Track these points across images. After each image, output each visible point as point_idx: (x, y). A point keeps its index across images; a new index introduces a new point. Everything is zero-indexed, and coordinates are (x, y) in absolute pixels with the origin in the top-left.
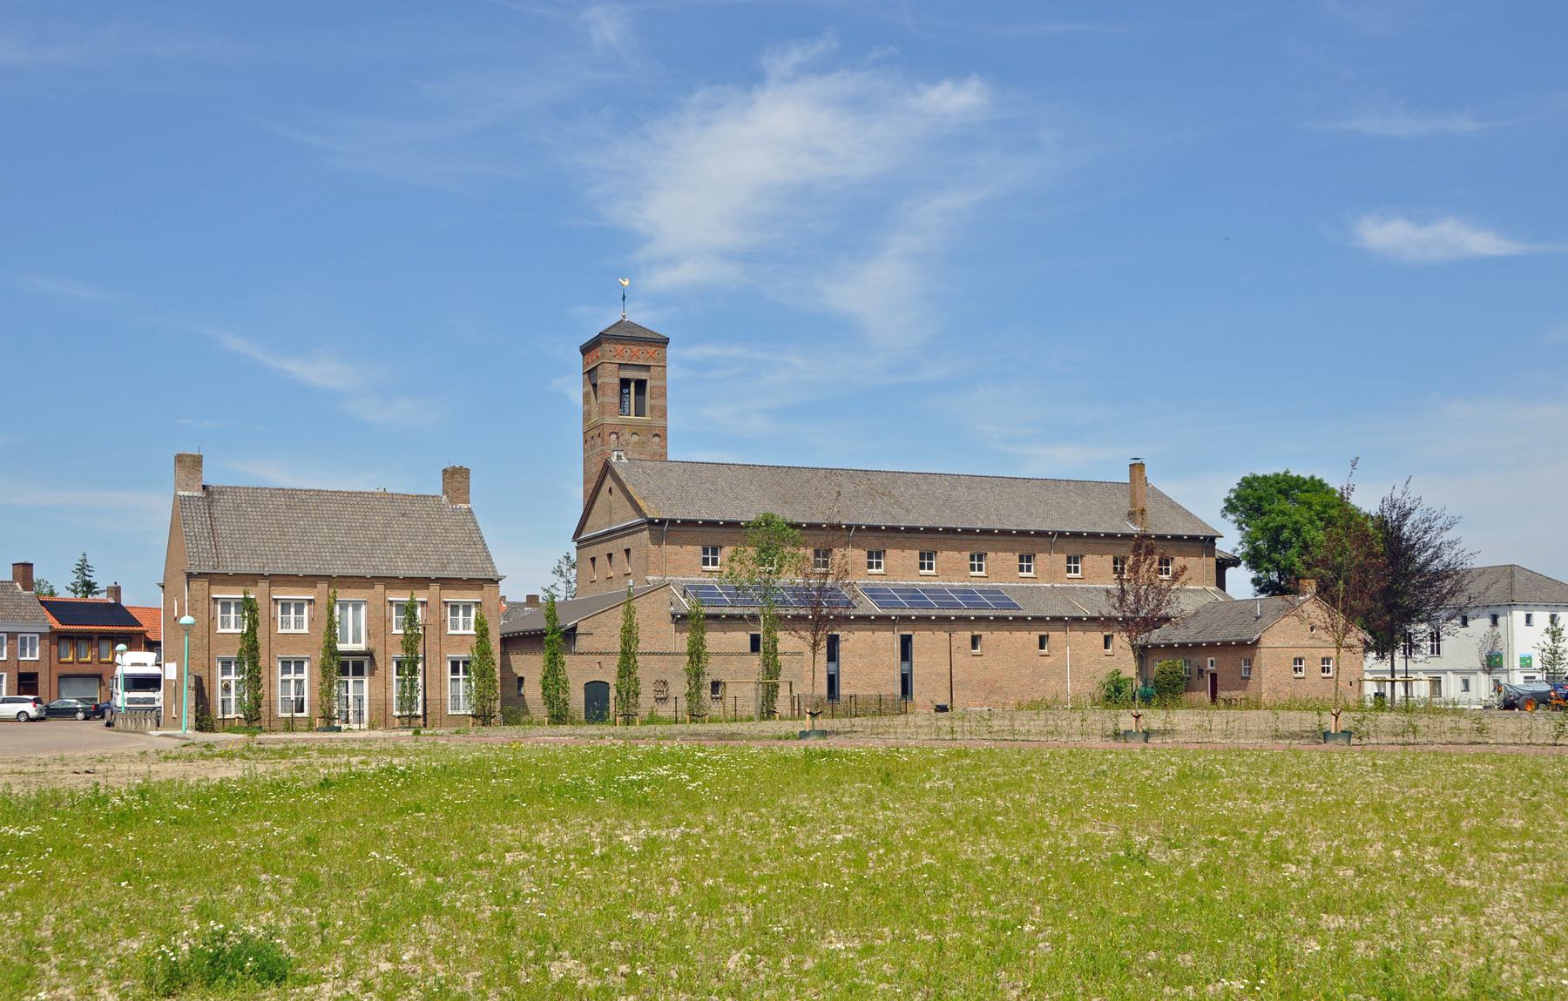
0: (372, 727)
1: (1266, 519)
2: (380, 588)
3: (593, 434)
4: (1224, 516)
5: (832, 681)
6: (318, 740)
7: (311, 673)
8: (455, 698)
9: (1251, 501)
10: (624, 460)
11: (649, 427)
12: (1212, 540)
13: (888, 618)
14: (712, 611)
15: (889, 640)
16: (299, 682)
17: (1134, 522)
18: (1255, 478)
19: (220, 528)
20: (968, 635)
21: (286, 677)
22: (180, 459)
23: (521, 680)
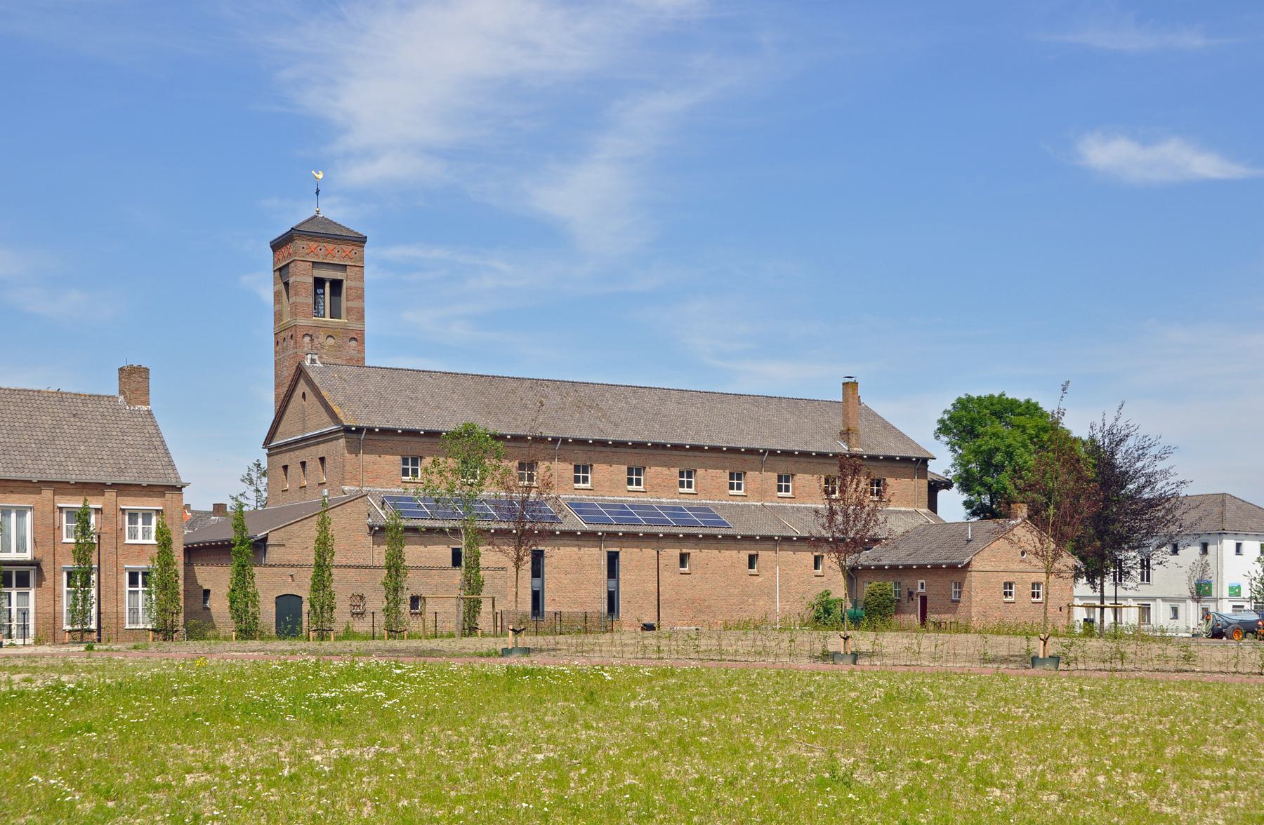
2: (47, 493)
4: (937, 438)
5: (537, 597)
8: (134, 611)
9: (965, 423)
10: (319, 364)
11: (345, 330)
12: (924, 461)
14: (411, 523)
15: (596, 556)
20: (744, 556)
23: (207, 592)
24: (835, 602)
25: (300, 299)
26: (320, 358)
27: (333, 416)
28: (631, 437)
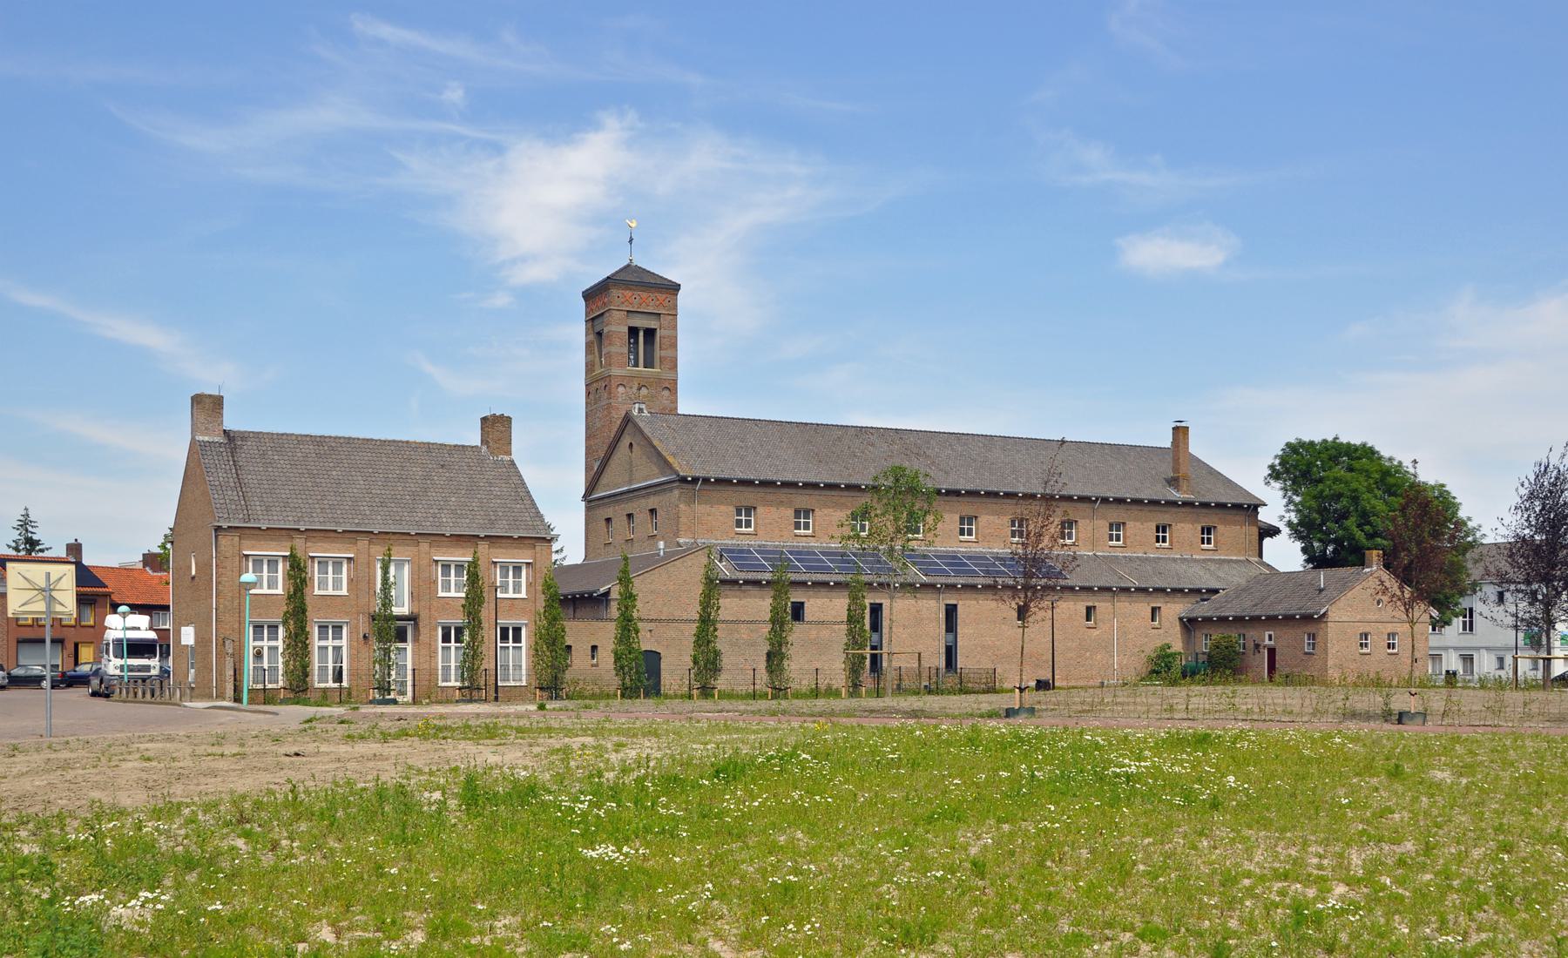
0: (415, 701)
1: (1320, 486)
2: (424, 546)
3: (597, 387)
4: (1267, 483)
5: (950, 653)
6: (461, 715)
7: (350, 640)
8: (446, 669)
9: (1301, 466)
10: (646, 413)
12: (1256, 507)
13: (933, 586)
14: (751, 576)
15: (933, 608)
16: (337, 649)
17: (1177, 488)
18: (1301, 444)
19: (248, 478)
21: (323, 643)
22: (197, 400)
24: (1173, 655)
25: (613, 349)
26: (648, 407)
27: (666, 465)
28: (962, 486)
